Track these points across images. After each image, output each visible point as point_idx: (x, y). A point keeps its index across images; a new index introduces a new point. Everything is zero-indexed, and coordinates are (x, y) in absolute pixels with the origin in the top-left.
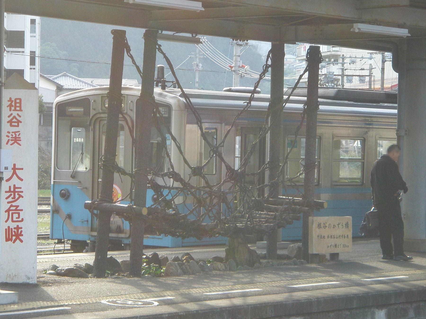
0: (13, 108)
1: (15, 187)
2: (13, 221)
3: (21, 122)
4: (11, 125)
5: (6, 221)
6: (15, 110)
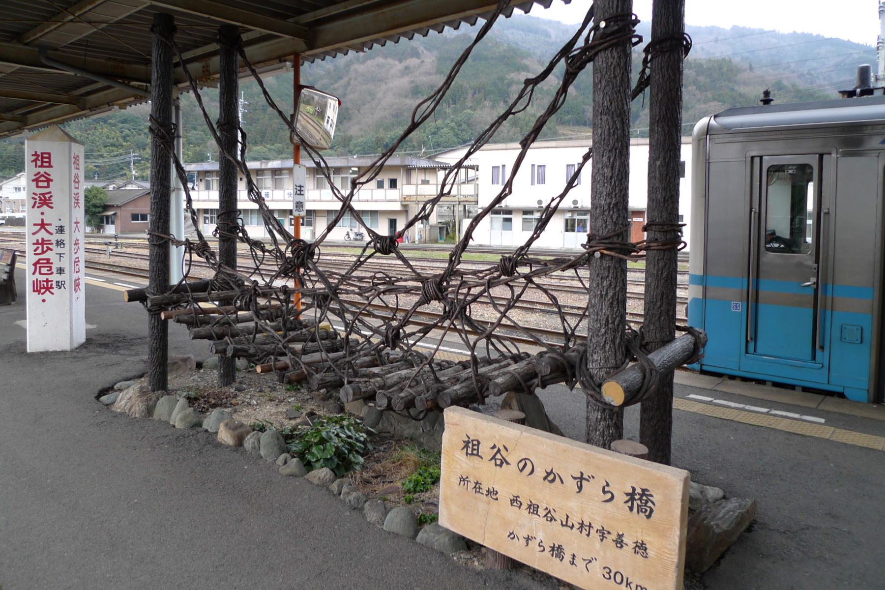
0: (39, 163)
1: (43, 239)
2: (40, 273)
3: (52, 180)
4: (37, 186)
5: (34, 274)
6: (42, 166)
